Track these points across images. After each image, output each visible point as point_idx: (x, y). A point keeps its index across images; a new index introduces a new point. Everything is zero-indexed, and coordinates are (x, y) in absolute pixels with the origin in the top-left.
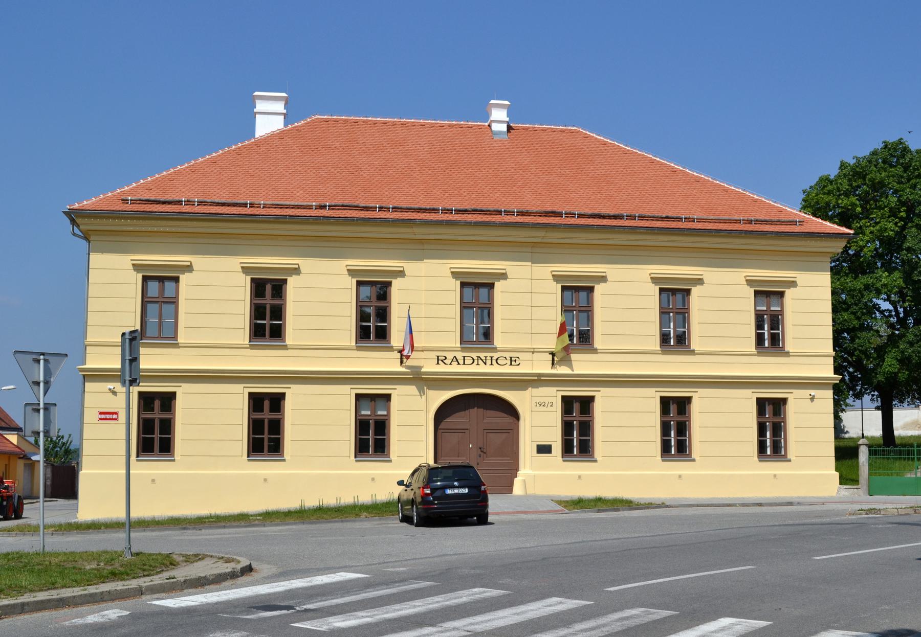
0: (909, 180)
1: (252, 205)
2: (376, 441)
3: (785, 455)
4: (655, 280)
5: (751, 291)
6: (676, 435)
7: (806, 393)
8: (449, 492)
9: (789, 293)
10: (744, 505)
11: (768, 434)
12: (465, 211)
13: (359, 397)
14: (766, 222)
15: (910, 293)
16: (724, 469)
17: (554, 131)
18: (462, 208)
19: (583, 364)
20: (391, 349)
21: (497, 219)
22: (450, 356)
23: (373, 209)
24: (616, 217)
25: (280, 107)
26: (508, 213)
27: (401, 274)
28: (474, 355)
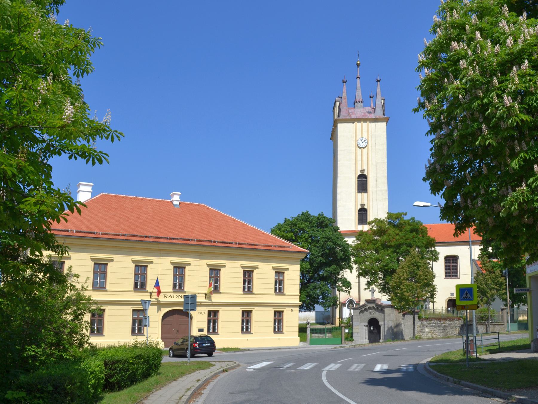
1: (96, 233)
2: (98, 328)
3: (217, 332)
4: (172, 263)
5: (274, 272)
7: (290, 309)
8: (204, 345)
9: (286, 273)
10: (275, 349)
12: (177, 239)
13: (133, 310)
14: (280, 247)
17: (195, 205)
19: (216, 298)
21: (188, 242)
22: (169, 294)
23: (143, 237)
24: (230, 243)
25: (90, 189)
26: (192, 240)
27: (152, 262)
28: (178, 294)
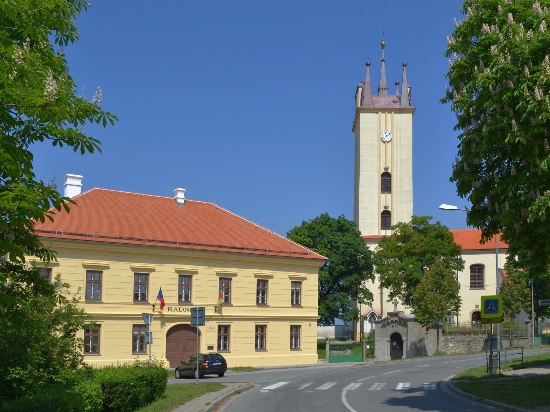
0: (331, 231)
1: (89, 236)
2: (93, 346)
3: (265, 349)
6: (260, 342)
7: (308, 323)
8: (214, 364)
9: (304, 282)
11: (222, 341)
12: (182, 243)
13: (134, 325)
15: (331, 280)
16: (278, 354)
17: (203, 204)
18: (181, 242)
19: (227, 312)
20: (149, 304)
21: (195, 247)
22: (174, 307)
23: (144, 240)
25: (79, 183)
26: (200, 245)
28: (184, 307)
